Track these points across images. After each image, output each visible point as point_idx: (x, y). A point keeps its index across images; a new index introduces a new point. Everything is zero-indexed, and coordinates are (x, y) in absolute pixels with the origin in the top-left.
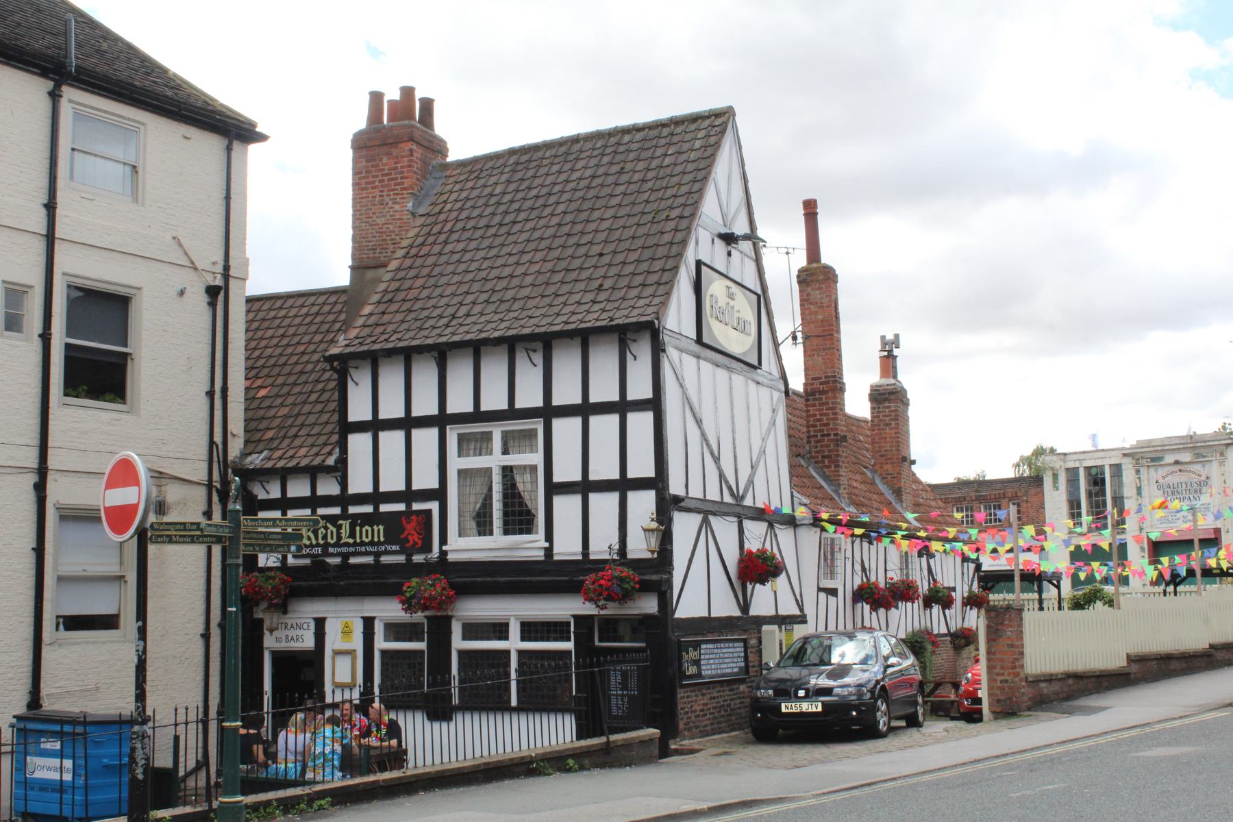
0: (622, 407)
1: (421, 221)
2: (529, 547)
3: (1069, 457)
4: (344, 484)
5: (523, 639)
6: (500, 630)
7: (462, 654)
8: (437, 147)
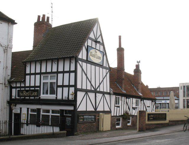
0: (70, 72)
1: (44, 38)
2: (53, 97)
4: (25, 85)
6: (48, 111)
7: (42, 115)
8: (51, 25)
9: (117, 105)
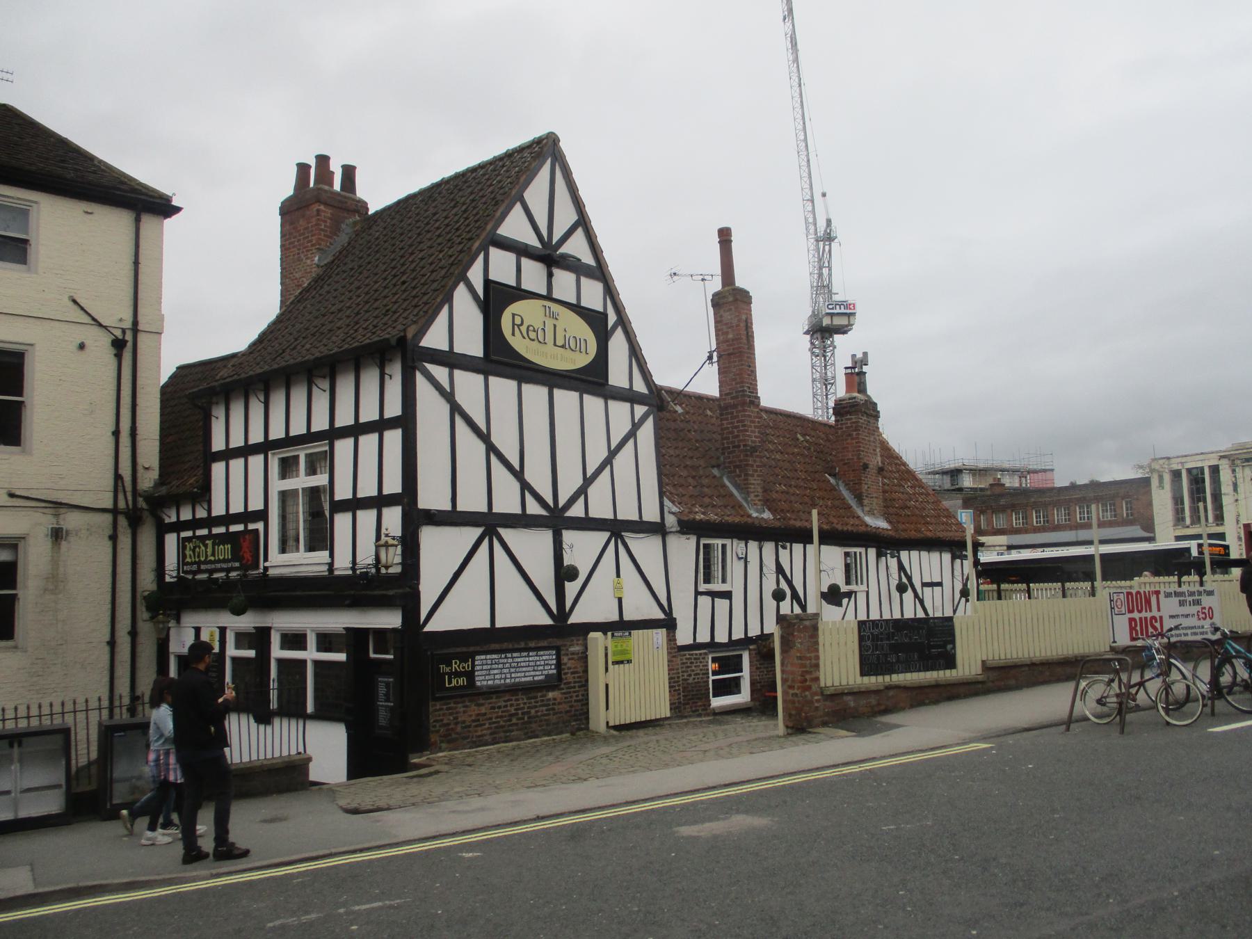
0: (381, 426)
3: (1173, 461)
5: (319, 649)
6: (295, 640)
7: (280, 661)
8: (363, 205)
9: (717, 586)
